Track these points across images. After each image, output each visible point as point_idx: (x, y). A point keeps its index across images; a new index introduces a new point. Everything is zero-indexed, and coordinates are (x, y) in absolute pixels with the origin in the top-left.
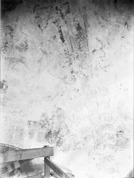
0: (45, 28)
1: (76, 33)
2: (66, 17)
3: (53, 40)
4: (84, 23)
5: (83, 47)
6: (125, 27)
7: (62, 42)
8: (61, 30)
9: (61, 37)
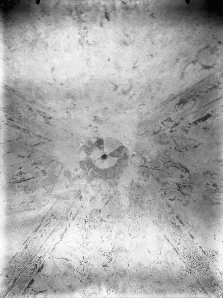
0: (196, 141)
1: (193, 102)
2: (177, 121)
3: (210, 130)
4: (172, 100)
5: (210, 85)
6: (139, 65)
7: (210, 118)
8: (193, 123)
9: (203, 121)
